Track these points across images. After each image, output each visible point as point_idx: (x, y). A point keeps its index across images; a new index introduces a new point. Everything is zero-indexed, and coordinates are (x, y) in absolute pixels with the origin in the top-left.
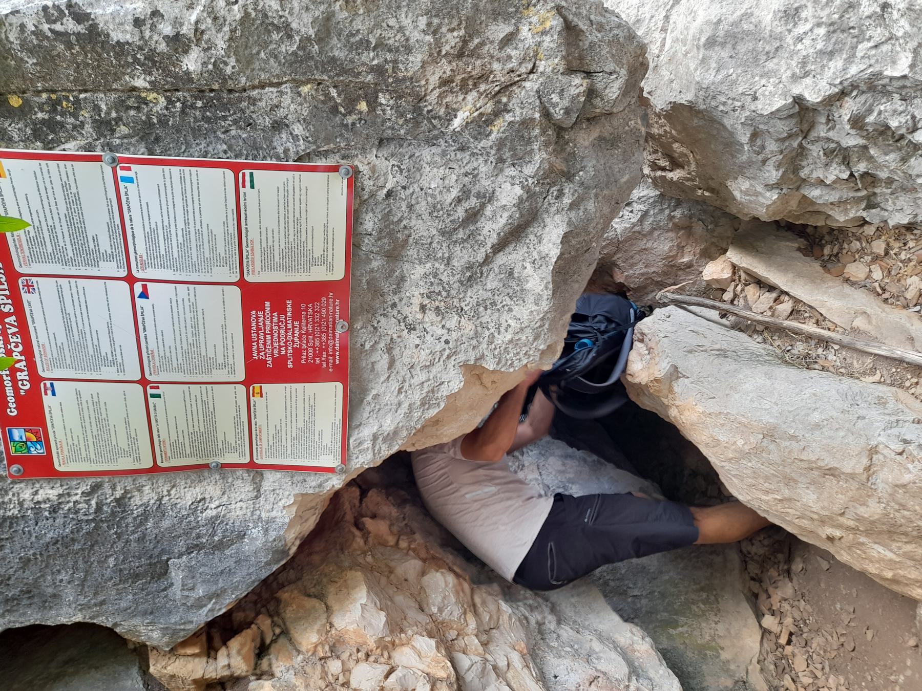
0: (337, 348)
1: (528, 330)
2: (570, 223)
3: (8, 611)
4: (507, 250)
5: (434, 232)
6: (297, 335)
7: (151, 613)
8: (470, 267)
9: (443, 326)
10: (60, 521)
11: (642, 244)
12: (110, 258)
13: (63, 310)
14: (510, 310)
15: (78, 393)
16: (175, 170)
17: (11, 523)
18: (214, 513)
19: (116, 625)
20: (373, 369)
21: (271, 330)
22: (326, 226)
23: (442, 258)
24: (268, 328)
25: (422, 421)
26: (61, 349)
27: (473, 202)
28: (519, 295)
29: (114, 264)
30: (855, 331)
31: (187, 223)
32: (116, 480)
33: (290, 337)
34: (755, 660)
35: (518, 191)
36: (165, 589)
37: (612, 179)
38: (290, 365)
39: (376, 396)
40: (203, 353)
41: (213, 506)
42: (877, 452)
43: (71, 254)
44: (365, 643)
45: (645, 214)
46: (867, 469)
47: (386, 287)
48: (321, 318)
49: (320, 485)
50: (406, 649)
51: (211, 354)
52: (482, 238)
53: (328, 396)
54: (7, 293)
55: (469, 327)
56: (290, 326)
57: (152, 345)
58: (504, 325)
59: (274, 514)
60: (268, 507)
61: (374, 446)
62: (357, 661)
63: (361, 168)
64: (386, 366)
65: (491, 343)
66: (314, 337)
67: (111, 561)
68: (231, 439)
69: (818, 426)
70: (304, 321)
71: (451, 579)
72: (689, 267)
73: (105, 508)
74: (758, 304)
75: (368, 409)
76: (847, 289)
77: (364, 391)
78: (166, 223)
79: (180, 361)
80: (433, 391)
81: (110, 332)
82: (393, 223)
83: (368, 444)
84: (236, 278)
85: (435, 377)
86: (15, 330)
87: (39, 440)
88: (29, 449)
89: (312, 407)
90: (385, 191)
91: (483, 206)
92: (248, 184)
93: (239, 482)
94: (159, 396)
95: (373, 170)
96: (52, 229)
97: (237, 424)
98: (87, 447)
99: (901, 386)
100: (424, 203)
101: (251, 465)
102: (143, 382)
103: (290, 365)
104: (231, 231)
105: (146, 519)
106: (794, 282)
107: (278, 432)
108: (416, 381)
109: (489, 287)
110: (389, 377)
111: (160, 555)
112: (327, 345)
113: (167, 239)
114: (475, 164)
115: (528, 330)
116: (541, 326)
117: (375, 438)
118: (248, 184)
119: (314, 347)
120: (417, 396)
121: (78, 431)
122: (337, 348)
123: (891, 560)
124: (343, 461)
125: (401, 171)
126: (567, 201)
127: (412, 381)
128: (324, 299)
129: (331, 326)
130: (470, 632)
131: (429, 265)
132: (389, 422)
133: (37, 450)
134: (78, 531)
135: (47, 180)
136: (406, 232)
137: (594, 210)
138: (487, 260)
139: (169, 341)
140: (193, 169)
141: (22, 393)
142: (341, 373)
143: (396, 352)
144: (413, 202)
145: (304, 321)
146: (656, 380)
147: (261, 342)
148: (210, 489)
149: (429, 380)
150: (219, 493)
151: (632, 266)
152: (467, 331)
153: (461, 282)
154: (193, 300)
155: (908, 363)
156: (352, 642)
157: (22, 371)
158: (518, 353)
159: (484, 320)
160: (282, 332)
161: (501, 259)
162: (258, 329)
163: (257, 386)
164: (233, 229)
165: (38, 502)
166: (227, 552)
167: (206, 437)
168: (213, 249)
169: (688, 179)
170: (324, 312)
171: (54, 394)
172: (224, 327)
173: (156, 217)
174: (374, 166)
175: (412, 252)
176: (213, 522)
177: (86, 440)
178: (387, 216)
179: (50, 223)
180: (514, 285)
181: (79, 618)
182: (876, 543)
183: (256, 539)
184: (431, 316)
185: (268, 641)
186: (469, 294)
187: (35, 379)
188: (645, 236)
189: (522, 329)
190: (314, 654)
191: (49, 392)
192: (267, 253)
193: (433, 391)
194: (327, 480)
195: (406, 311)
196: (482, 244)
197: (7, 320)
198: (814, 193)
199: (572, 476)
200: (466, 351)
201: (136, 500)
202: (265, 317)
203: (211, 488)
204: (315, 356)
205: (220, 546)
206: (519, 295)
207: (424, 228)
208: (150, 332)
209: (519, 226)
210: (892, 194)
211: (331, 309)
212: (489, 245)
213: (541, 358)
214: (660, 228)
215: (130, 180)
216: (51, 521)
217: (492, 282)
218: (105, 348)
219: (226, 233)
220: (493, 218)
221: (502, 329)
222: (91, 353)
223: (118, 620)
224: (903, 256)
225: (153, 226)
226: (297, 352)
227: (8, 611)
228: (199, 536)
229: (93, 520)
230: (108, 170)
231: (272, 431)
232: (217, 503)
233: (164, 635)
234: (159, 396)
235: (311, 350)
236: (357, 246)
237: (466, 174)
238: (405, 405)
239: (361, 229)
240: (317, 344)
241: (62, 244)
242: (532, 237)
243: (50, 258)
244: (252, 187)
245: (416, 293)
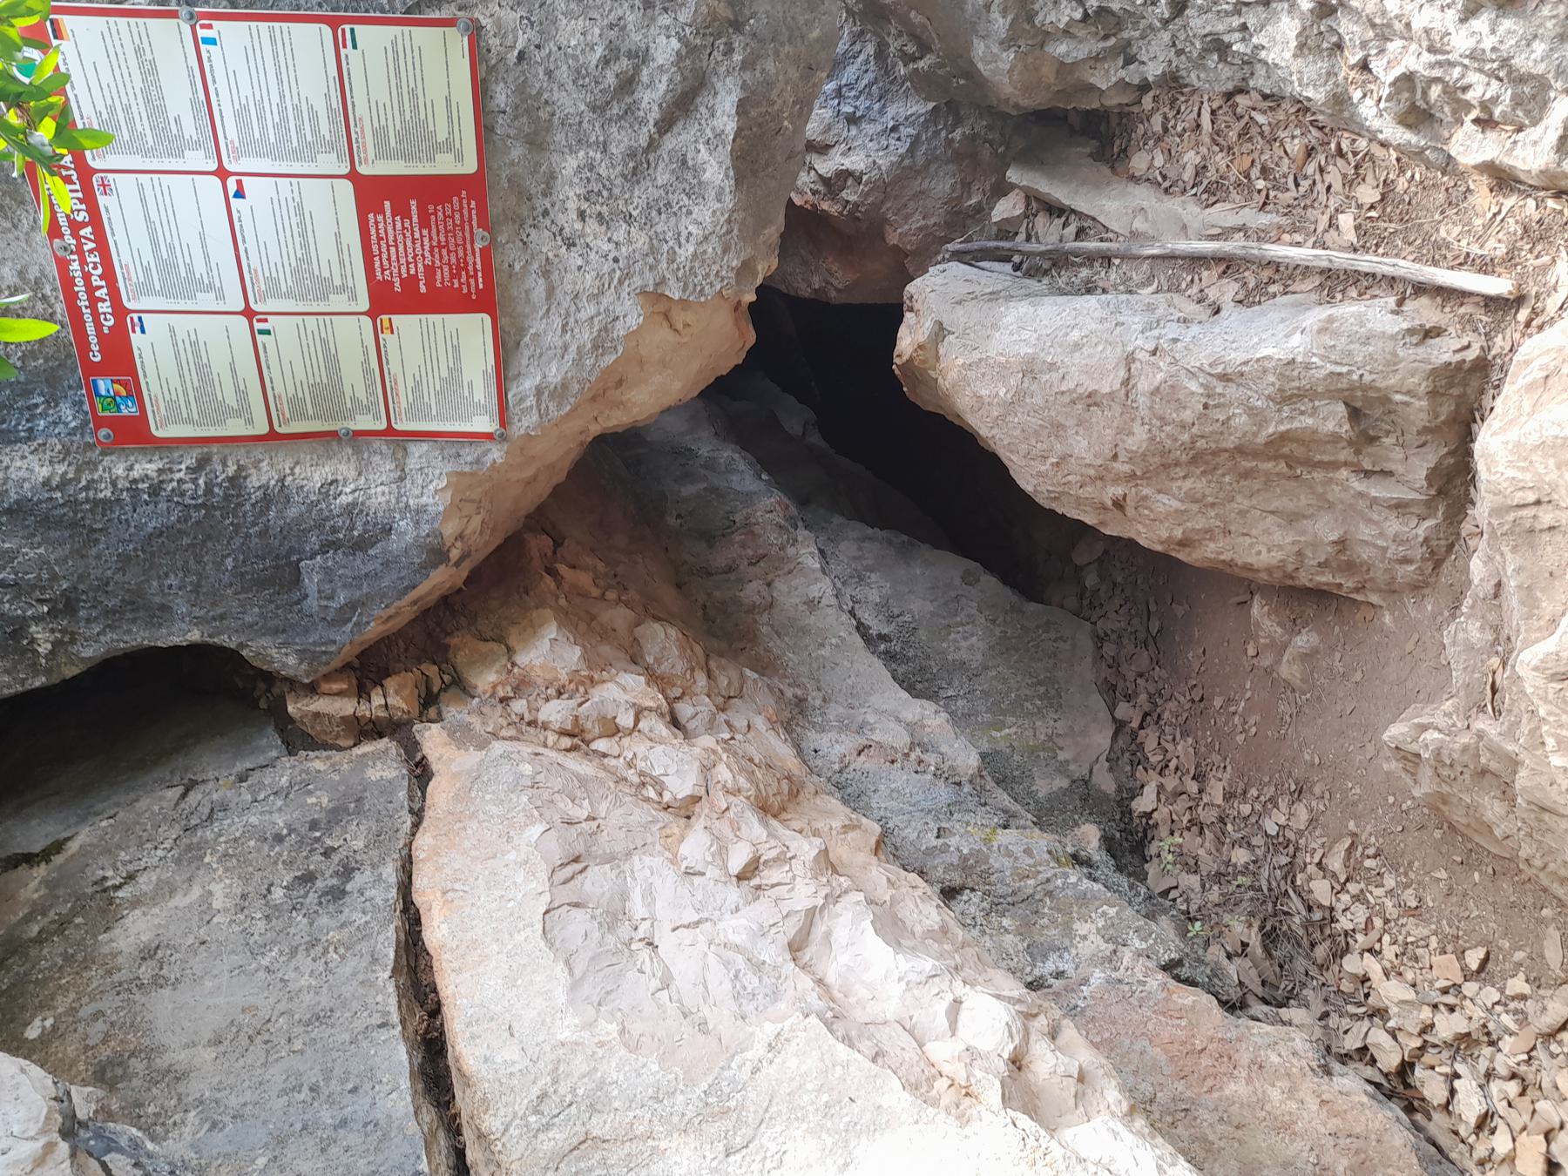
0: (479, 267)
1: (714, 239)
2: (744, 86)
3: (109, 626)
4: (675, 130)
5: (583, 107)
6: (427, 248)
7: (284, 631)
8: (632, 154)
9: (609, 240)
10: (163, 506)
11: (916, 185)
12: (197, 145)
13: (147, 217)
14: (689, 213)
15: (172, 330)
16: (263, 26)
17: (104, 510)
18: (350, 498)
19: (242, 645)
20: (528, 301)
21: (395, 241)
22: (448, 100)
23: (597, 142)
24: (391, 238)
25: (597, 372)
26: (147, 270)
27: (624, 63)
28: (696, 191)
29: (201, 153)
30: (1134, 235)
31: (282, 97)
32: (227, 451)
33: (419, 251)
34: (1104, 757)
35: (675, 44)
36: (298, 602)
37: (797, 33)
38: (423, 289)
39: (537, 335)
40: (317, 272)
41: (348, 490)
42: (1134, 360)
43: (151, 142)
44: (557, 679)
45: (915, 142)
46: (1126, 382)
47: (535, 189)
48: (455, 225)
49: (478, 461)
50: (610, 685)
51: (325, 274)
52: (642, 113)
53: (473, 330)
54: (80, 195)
55: (641, 240)
56: (417, 235)
57: (255, 263)
58: (684, 234)
59: (424, 500)
60: (417, 492)
61: (539, 405)
62: (547, 700)
63: (484, 22)
64: (543, 295)
65: (671, 261)
66: (449, 252)
67: (229, 562)
68: (361, 394)
69: (1077, 346)
70: (434, 231)
71: (673, 632)
72: (979, 212)
73: (216, 490)
74: (1050, 234)
75: (527, 353)
76: (1131, 187)
77: (522, 331)
78: (258, 97)
79: (290, 283)
80: (606, 329)
81: (204, 246)
82: (530, 96)
83: (531, 401)
84: (345, 170)
85: (607, 310)
86: (92, 245)
87: (129, 395)
88: (118, 407)
89: (456, 348)
90: (516, 53)
91: (637, 69)
92: (349, 43)
93: (376, 459)
94: (268, 332)
95: (498, 24)
96: (127, 109)
97: (367, 371)
98: (188, 403)
99: (1178, 290)
100: (565, 68)
101: (390, 431)
102: (248, 313)
103: (423, 289)
104: (335, 106)
105: (268, 509)
106: (1076, 192)
107: (418, 384)
108: (583, 315)
109: (660, 183)
110: (548, 310)
111: (288, 556)
112: (466, 263)
113: (261, 118)
114: (620, 12)
115: (714, 239)
116: (729, 232)
117: (539, 392)
118: (349, 43)
119: (449, 264)
120: (586, 336)
121: (175, 382)
122: (479, 267)
123: (1176, 511)
124: (503, 423)
125: (532, 24)
126: (737, 57)
127: (578, 316)
128: (455, 199)
129: (468, 235)
130: (698, 690)
131: (581, 154)
132: (554, 370)
133: (129, 409)
134: (186, 521)
135: (117, 43)
136: (548, 109)
137: (773, 71)
138: (652, 145)
139: (275, 257)
140: (284, 25)
141: (106, 331)
142: (483, 302)
143: (555, 277)
144: (552, 67)
145: (434, 231)
146: (921, 347)
147: (385, 256)
148: (342, 468)
149: (599, 314)
150: (353, 474)
151: (907, 217)
152: (639, 245)
153: (624, 176)
154: (297, 199)
155: (1183, 258)
156: (539, 681)
157: (104, 301)
158: (708, 275)
159: (659, 228)
160: (409, 243)
161: (670, 142)
162: (379, 239)
163: (385, 317)
164: (336, 103)
165: (135, 481)
166: (371, 552)
167: (328, 393)
168: (316, 130)
169: (941, 65)
170: (457, 216)
171: (143, 331)
172: (338, 235)
173: (246, 90)
174: (499, 18)
175: (559, 137)
176: (349, 509)
177: (185, 393)
178: (521, 89)
179: (125, 101)
180: (690, 177)
181: (195, 636)
182: (1159, 492)
183: (405, 533)
184: (592, 226)
185: (435, 690)
186: (637, 193)
187: (120, 311)
188: (918, 172)
189: (706, 238)
190: (493, 695)
191: (138, 329)
192: (380, 134)
193: (606, 329)
194: (485, 454)
195: (561, 219)
196: (643, 122)
197: (82, 233)
198: (1061, 48)
199: (870, 562)
200: (641, 273)
201: (254, 481)
202: (385, 222)
203: (341, 467)
204: (452, 276)
205: (360, 546)
206: (696, 191)
207: (569, 102)
208: (251, 244)
209: (684, 95)
210: (1143, 38)
211: (465, 212)
212: (652, 122)
213: (738, 283)
214: (936, 158)
215: (212, 41)
216: (151, 507)
217: (663, 177)
218: (200, 268)
219: (329, 107)
220: (650, 85)
221: (683, 240)
222: (183, 274)
223: (243, 639)
224: (1179, 129)
225: (244, 101)
226: (430, 271)
227: (109, 626)
228: (334, 530)
229: (203, 505)
230: (186, 28)
231: (410, 383)
232: (352, 486)
233: (301, 661)
234: (268, 332)
235: (446, 269)
236: (491, 129)
237: (611, 26)
238: (573, 348)
239: (492, 105)
240: (454, 260)
241: (140, 129)
242: (703, 110)
243: (130, 149)
244: (355, 47)
245: (571, 194)
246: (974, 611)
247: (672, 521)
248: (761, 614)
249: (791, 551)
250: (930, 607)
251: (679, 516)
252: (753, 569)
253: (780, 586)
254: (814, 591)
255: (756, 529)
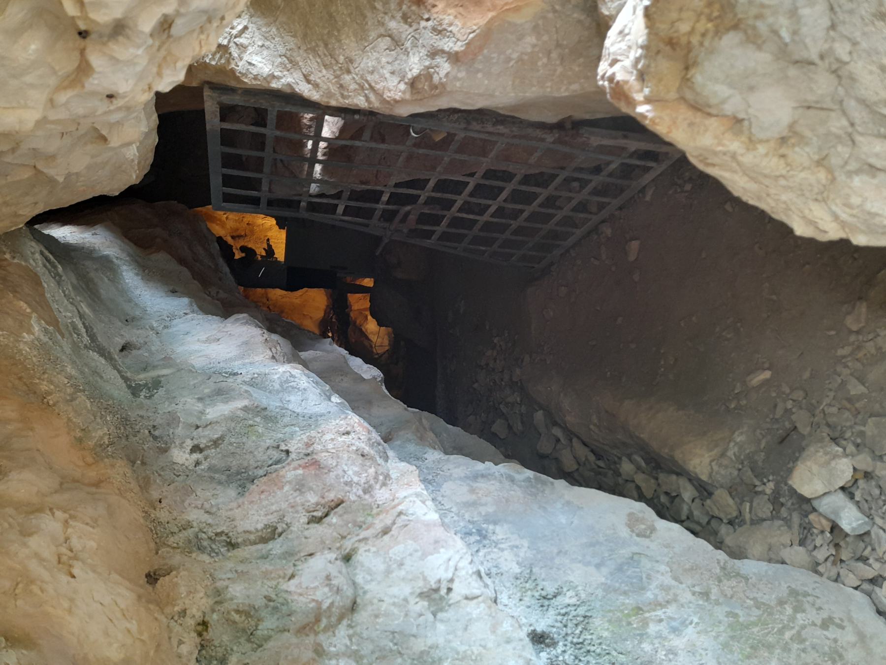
246: (668, 580)
247: (181, 456)
248: (331, 628)
249: (381, 495)
250: (599, 577)
251: (196, 449)
252: (317, 530)
253: (369, 559)
254: (437, 567)
255: (323, 457)
